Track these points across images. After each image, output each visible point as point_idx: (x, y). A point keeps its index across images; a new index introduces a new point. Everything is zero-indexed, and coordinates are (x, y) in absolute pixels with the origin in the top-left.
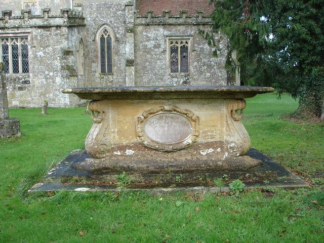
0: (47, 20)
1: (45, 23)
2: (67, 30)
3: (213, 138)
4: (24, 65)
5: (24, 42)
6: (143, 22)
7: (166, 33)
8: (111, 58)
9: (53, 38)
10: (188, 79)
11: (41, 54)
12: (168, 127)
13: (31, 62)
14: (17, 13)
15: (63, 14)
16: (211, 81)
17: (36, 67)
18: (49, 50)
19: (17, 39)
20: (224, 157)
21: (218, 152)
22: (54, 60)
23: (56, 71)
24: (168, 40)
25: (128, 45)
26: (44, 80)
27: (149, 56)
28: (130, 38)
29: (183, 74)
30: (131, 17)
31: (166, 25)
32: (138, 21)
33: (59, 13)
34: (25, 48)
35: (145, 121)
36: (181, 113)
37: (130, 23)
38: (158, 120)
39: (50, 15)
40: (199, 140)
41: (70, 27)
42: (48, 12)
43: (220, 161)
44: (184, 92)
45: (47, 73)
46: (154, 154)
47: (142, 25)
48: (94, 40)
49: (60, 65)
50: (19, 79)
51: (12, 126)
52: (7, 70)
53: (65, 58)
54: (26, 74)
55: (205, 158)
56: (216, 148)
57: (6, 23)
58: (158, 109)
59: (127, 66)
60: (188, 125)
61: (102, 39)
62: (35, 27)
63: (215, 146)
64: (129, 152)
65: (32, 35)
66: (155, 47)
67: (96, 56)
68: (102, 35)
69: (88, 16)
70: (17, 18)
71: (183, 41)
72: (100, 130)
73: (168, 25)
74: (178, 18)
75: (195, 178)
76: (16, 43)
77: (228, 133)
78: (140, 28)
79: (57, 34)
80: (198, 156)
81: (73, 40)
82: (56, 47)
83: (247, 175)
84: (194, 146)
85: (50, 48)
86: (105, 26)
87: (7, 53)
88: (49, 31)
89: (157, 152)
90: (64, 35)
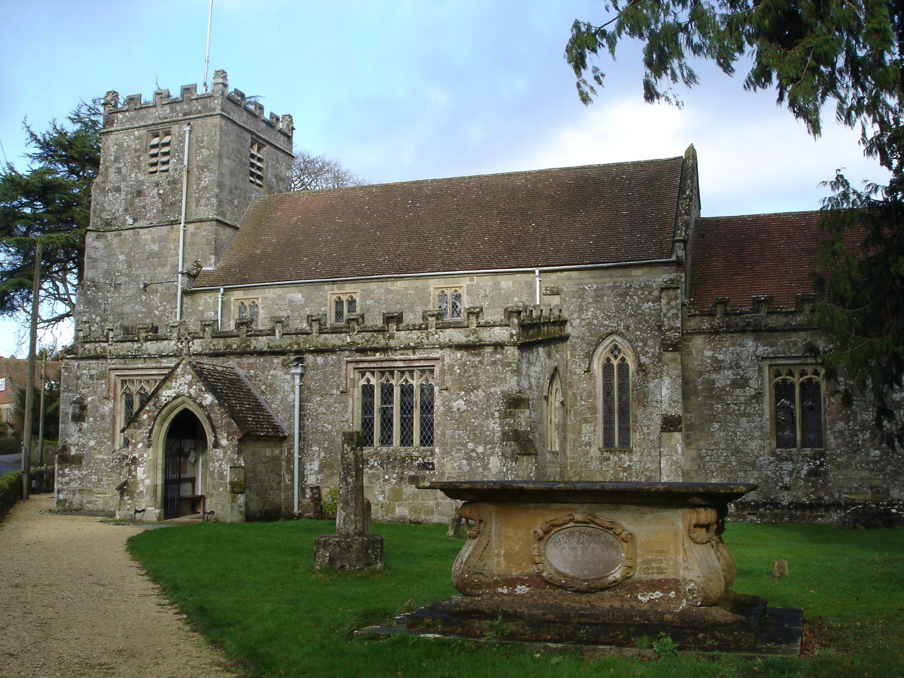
0: (475, 332)
1: (472, 338)
2: (516, 353)
3: (662, 573)
4: (424, 429)
5: (427, 380)
6: (706, 326)
7: (762, 350)
8: (628, 412)
9: (486, 371)
10: (821, 465)
11: (460, 404)
12: (583, 549)
13: (439, 423)
14: (409, 318)
15: (509, 318)
16: (882, 470)
17: (449, 432)
18: (477, 396)
19: (411, 372)
20: (681, 607)
21: (670, 598)
22: (487, 418)
23: (492, 442)
24: (766, 368)
25: (667, 381)
26: (465, 462)
27: (719, 407)
28: (673, 365)
29: (808, 451)
30: (675, 316)
31: (760, 330)
32: (693, 323)
33: (499, 317)
34: (427, 392)
35: (546, 538)
36: (603, 527)
37: (671, 328)
38: (568, 537)
39: (482, 322)
40: (637, 575)
41: (525, 347)
42: (477, 315)
43: (669, 612)
44: (595, 491)
45: (471, 445)
46: (559, 595)
47: (700, 332)
48: (588, 371)
49: (499, 429)
50: (412, 460)
51: (367, 550)
52: (389, 437)
53: (511, 415)
54: (427, 448)
55: (646, 607)
56: (668, 591)
57: (389, 338)
58: (565, 518)
59: (663, 430)
60: (617, 547)
61: (607, 368)
62: (450, 347)
63: (666, 587)
64: (521, 589)
65: (443, 365)
66: (735, 384)
67: (593, 409)
68: (608, 359)
69: (575, 316)
70: (414, 328)
71: (805, 368)
72: (475, 548)
73: (766, 331)
74: (791, 313)
75: (611, 634)
76: (411, 381)
77: (686, 565)
78: (698, 341)
79: (494, 363)
80: (634, 603)
81: (533, 374)
82: (492, 390)
83: (701, 635)
84: (626, 584)
85: (480, 393)
86: (614, 337)
87: (390, 403)
88: (478, 355)
89: (564, 592)
90: (509, 364)
